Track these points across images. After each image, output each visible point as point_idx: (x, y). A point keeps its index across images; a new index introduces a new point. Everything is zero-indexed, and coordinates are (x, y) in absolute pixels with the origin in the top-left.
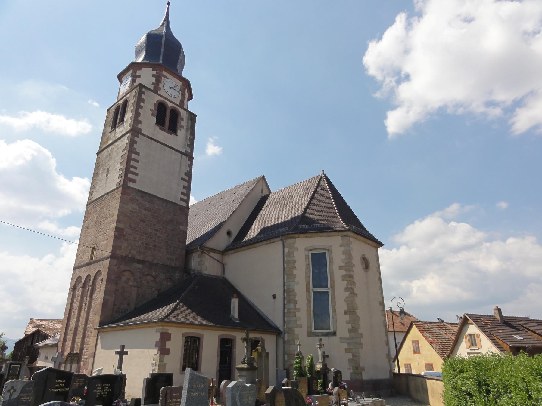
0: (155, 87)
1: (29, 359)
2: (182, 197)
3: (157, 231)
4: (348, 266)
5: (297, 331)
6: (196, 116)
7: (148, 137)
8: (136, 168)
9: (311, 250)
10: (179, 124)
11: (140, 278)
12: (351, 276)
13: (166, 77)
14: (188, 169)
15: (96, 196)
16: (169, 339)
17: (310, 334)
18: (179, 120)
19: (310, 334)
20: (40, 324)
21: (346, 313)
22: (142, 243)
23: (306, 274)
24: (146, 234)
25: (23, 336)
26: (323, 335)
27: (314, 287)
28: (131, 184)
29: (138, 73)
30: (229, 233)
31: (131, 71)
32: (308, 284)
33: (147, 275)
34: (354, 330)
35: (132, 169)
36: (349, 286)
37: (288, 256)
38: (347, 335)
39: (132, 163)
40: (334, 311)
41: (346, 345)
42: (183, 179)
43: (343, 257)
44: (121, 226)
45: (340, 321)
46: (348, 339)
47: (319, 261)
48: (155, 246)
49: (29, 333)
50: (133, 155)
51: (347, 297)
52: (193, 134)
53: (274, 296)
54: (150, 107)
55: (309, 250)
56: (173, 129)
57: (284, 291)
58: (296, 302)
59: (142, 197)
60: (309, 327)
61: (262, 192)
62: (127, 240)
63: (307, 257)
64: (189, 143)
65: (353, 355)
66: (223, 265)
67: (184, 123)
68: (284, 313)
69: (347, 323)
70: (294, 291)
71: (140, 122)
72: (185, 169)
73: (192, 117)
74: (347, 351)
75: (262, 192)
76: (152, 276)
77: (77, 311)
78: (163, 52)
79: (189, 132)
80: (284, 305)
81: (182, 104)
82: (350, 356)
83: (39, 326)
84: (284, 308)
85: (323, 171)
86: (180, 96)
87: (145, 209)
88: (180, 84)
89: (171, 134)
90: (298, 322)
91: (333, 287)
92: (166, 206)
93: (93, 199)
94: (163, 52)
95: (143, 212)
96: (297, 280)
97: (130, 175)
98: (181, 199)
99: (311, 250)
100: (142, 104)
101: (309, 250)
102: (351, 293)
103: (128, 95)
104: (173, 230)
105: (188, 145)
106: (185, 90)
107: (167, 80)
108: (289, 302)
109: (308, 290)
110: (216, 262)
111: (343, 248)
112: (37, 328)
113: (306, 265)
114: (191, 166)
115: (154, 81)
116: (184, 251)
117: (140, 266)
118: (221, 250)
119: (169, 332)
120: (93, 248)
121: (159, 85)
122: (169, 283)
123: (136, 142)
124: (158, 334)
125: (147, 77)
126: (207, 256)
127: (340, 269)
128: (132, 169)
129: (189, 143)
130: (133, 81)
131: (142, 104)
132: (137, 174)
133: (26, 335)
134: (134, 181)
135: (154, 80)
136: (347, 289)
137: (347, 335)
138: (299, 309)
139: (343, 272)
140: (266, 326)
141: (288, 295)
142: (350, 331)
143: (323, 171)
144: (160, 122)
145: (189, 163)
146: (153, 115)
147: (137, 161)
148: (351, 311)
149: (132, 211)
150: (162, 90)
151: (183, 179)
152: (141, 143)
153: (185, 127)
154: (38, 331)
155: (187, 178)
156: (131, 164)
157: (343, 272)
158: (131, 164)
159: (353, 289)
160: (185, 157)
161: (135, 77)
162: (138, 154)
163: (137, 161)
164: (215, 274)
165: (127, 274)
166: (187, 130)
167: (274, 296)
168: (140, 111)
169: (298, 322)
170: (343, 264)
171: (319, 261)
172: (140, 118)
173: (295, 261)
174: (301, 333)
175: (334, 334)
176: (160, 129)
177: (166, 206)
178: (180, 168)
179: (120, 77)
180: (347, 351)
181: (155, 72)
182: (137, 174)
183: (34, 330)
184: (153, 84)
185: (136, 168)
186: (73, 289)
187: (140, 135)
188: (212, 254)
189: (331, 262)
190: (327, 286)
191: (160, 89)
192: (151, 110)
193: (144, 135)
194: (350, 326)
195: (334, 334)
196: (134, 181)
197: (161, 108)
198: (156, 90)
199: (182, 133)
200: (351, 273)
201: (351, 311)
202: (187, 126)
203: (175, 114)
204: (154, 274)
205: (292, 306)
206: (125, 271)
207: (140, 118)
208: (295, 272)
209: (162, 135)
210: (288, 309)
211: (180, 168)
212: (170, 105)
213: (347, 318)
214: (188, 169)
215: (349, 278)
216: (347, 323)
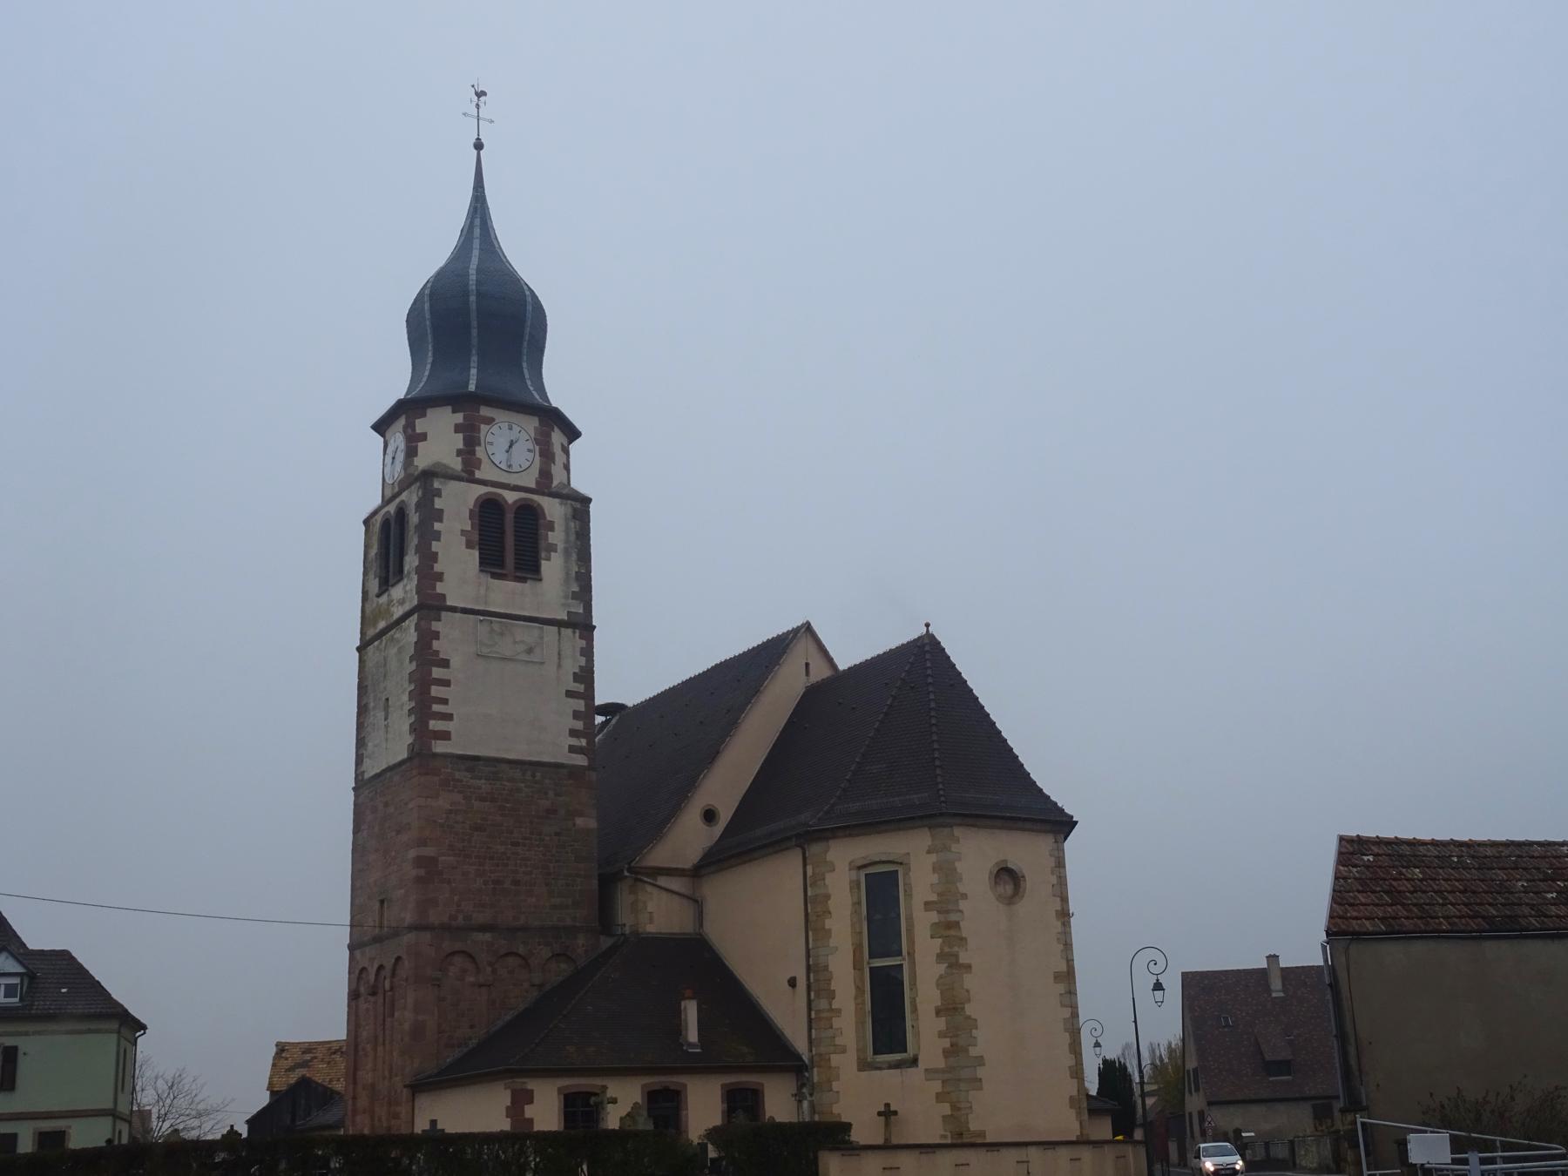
0: (465, 463)
1: (520, 1136)
2: (574, 742)
3: (516, 844)
4: (946, 901)
5: (835, 1059)
6: (589, 500)
7: (465, 611)
8: (445, 701)
9: (864, 866)
10: (542, 544)
11: (490, 964)
12: (955, 925)
13: (490, 421)
14: (583, 661)
15: (372, 769)
16: (531, 1101)
17: (864, 1066)
18: (542, 531)
19: (864, 1066)
20: (308, 1057)
21: (938, 1013)
22: (485, 883)
23: (853, 925)
24: (492, 858)
25: (263, 1099)
26: (890, 1067)
27: (871, 956)
28: (440, 747)
29: (421, 426)
30: (709, 816)
31: (402, 421)
32: (857, 949)
33: (507, 955)
34: (953, 1051)
35: (436, 708)
36: (947, 950)
37: (814, 884)
38: (941, 1063)
39: (436, 691)
40: (915, 1010)
41: (937, 1086)
42: (570, 694)
43: (935, 878)
44: (429, 851)
45: (926, 1030)
46: (943, 1071)
47: (881, 891)
48: (516, 883)
49: (281, 1086)
50: (435, 670)
51: (941, 977)
52: (584, 556)
53: (792, 983)
54: (458, 527)
55: (860, 868)
56: (528, 568)
57: (809, 968)
58: (831, 995)
59: (469, 770)
60: (861, 1050)
61: (807, 673)
62: (449, 882)
63: (855, 885)
64: (576, 589)
65: (955, 1108)
66: (697, 903)
67: (556, 537)
68: (810, 1020)
69: (942, 1035)
70: (826, 968)
71: (440, 577)
72: (572, 664)
73: (580, 506)
74: (940, 1097)
75: (807, 673)
76: (517, 954)
77: (369, 1047)
78: (478, 333)
79: (574, 557)
80: (809, 1002)
81: (545, 484)
82: (946, 1109)
83: (305, 1064)
84: (810, 1009)
85: (927, 625)
86: (537, 457)
87: (483, 799)
88: (531, 424)
89: (523, 580)
90: (838, 1041)
91: (911, 954)
92: (533, 776)
93: (367, 776)
94: (478, 333)
95: (476, 804)
96: (833, 942)
97: (435, 725)
98: (572, 749)
99: (864, 866)
100: (437, 526)
101: (860, 868)
102: (950, 966)
103: (404, 496)
104: (557, 834)
105: (575, 596)
106: (549, 436)
107: (495, 429)
108: (818, 996)
109: (857, 965)
110: (676, 898)
111: (933, 858)
112: (300, 1072)
113: (854, 904)
114: (588, 652)
115: (461, 445)
116: (595, 882)
117: (488, 936)
118: (688, 866)
119: (529, 1087)
120: (382, 902)
121: (473, 453)
122: (563, 966)
123: (436, 635)
124: (508, 1092)
125: (441, 437)
126: (649, 888)
127: (926, 910)
128: (436, 708)
129: (576, 589)
130: (411, 452)
131: (437, 526)
132: (448, 717)
133: (273, 1093)
134: (446, 736)
135: (458, 441)
136: (941, 957)
137: (941, 1063)
138: (839, 1011)
139: (934, 917)
140: (775, 1053)
141: (816, 979)
142: (947, 1053)
143: (927, 625)
144: (492, 562)
145: (583, 643)
146: (469, 545)
147: (446, 683)
148: (951, 1007)
149: (450, 812)
150: (485, 465)
151: (570, 694)
152: (452, 636)
153: (560, 546)
154: (304, 1083)
155: (581, 688)
156: (433, 694)
157: (934, 917)
158: (433, 694)
159: (957, 956)
160: (569, 631)
161: (414, 440)
162: (445, 664)
163: (446, 683)
164: (676, 930)
165: (458, 959)
166: (567, 552)
167: (792, 983)
168: (435, 546)
169: (838, 1041)
170: (934, 898)
171: (881, 891)
172: (437, 568)
173: (828, 897)
174: (845, 1063)
175: (914, 1062)
176: (495, 576)
177: (533, 776)
178: (559, 666)
179: (381, 427)
180: (940, 1097)
181: (459, 418)
182: (448, 717)
183: (293, 1078)
184: (459, 453)
185: (445, 701)
186: (354, 996)
187: (444, 614)
188: (663, 881)
189: (909, 895)
190: (899, 953)
191: (478, 464)
192: (463, 532)
193: (453, 609)
194: (946, 1043)
195: (914, 1062)
196: (446, 736)
197: (489, 512)
198: (468, 474)
199: (553, 568)
200: (953, 917)
201: (951, 1007)
202: (567, 541)
203: (529, 516)
204: (521, 950)
205: (823, 1004)
206: (453, 953)
207: (437, 568)
208: (828, 923)
209: (504, 594)
210: (818, 1012)
211: (559, 666)
212: (511, 497)
213: (941, 1023)
214: (583, 661)
215: (948, 930)
216: (942, 1035)
